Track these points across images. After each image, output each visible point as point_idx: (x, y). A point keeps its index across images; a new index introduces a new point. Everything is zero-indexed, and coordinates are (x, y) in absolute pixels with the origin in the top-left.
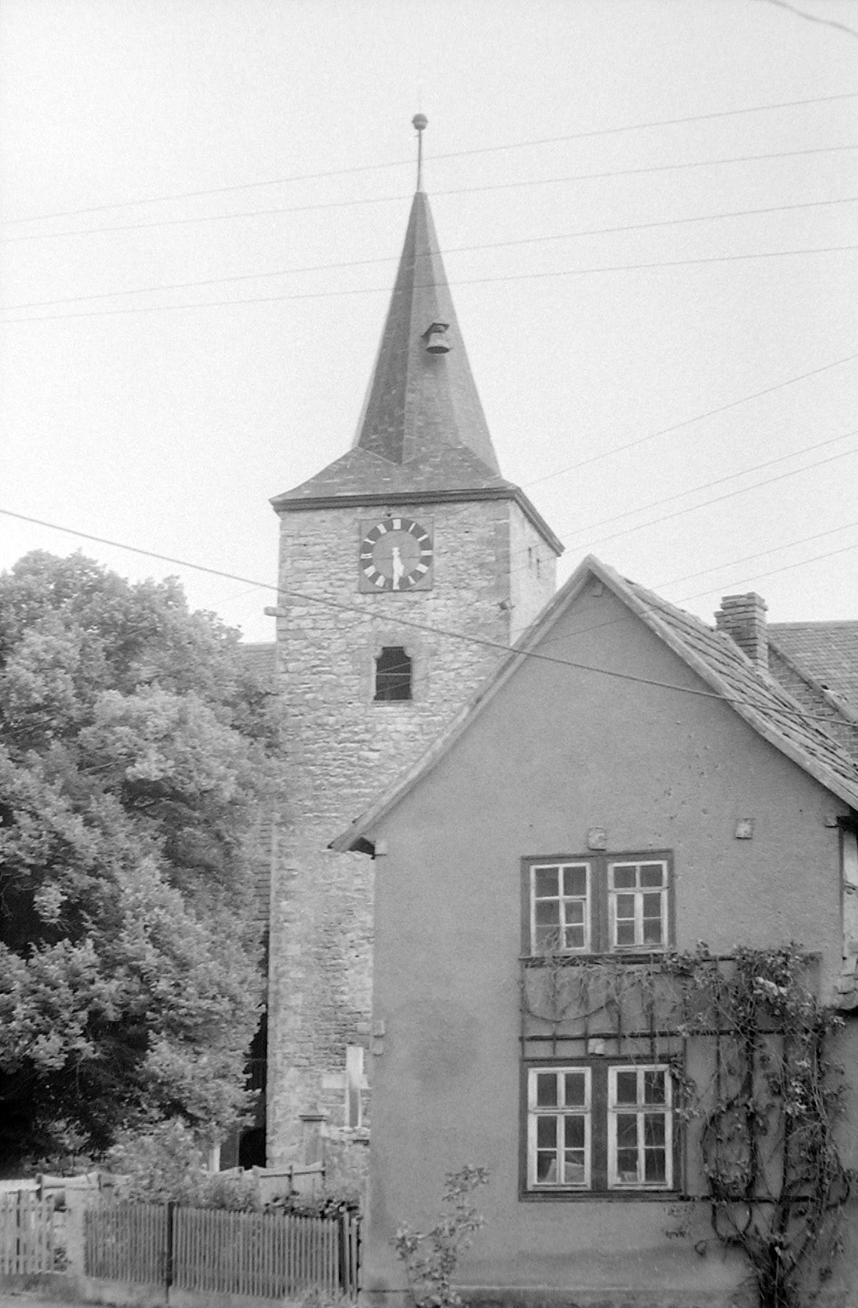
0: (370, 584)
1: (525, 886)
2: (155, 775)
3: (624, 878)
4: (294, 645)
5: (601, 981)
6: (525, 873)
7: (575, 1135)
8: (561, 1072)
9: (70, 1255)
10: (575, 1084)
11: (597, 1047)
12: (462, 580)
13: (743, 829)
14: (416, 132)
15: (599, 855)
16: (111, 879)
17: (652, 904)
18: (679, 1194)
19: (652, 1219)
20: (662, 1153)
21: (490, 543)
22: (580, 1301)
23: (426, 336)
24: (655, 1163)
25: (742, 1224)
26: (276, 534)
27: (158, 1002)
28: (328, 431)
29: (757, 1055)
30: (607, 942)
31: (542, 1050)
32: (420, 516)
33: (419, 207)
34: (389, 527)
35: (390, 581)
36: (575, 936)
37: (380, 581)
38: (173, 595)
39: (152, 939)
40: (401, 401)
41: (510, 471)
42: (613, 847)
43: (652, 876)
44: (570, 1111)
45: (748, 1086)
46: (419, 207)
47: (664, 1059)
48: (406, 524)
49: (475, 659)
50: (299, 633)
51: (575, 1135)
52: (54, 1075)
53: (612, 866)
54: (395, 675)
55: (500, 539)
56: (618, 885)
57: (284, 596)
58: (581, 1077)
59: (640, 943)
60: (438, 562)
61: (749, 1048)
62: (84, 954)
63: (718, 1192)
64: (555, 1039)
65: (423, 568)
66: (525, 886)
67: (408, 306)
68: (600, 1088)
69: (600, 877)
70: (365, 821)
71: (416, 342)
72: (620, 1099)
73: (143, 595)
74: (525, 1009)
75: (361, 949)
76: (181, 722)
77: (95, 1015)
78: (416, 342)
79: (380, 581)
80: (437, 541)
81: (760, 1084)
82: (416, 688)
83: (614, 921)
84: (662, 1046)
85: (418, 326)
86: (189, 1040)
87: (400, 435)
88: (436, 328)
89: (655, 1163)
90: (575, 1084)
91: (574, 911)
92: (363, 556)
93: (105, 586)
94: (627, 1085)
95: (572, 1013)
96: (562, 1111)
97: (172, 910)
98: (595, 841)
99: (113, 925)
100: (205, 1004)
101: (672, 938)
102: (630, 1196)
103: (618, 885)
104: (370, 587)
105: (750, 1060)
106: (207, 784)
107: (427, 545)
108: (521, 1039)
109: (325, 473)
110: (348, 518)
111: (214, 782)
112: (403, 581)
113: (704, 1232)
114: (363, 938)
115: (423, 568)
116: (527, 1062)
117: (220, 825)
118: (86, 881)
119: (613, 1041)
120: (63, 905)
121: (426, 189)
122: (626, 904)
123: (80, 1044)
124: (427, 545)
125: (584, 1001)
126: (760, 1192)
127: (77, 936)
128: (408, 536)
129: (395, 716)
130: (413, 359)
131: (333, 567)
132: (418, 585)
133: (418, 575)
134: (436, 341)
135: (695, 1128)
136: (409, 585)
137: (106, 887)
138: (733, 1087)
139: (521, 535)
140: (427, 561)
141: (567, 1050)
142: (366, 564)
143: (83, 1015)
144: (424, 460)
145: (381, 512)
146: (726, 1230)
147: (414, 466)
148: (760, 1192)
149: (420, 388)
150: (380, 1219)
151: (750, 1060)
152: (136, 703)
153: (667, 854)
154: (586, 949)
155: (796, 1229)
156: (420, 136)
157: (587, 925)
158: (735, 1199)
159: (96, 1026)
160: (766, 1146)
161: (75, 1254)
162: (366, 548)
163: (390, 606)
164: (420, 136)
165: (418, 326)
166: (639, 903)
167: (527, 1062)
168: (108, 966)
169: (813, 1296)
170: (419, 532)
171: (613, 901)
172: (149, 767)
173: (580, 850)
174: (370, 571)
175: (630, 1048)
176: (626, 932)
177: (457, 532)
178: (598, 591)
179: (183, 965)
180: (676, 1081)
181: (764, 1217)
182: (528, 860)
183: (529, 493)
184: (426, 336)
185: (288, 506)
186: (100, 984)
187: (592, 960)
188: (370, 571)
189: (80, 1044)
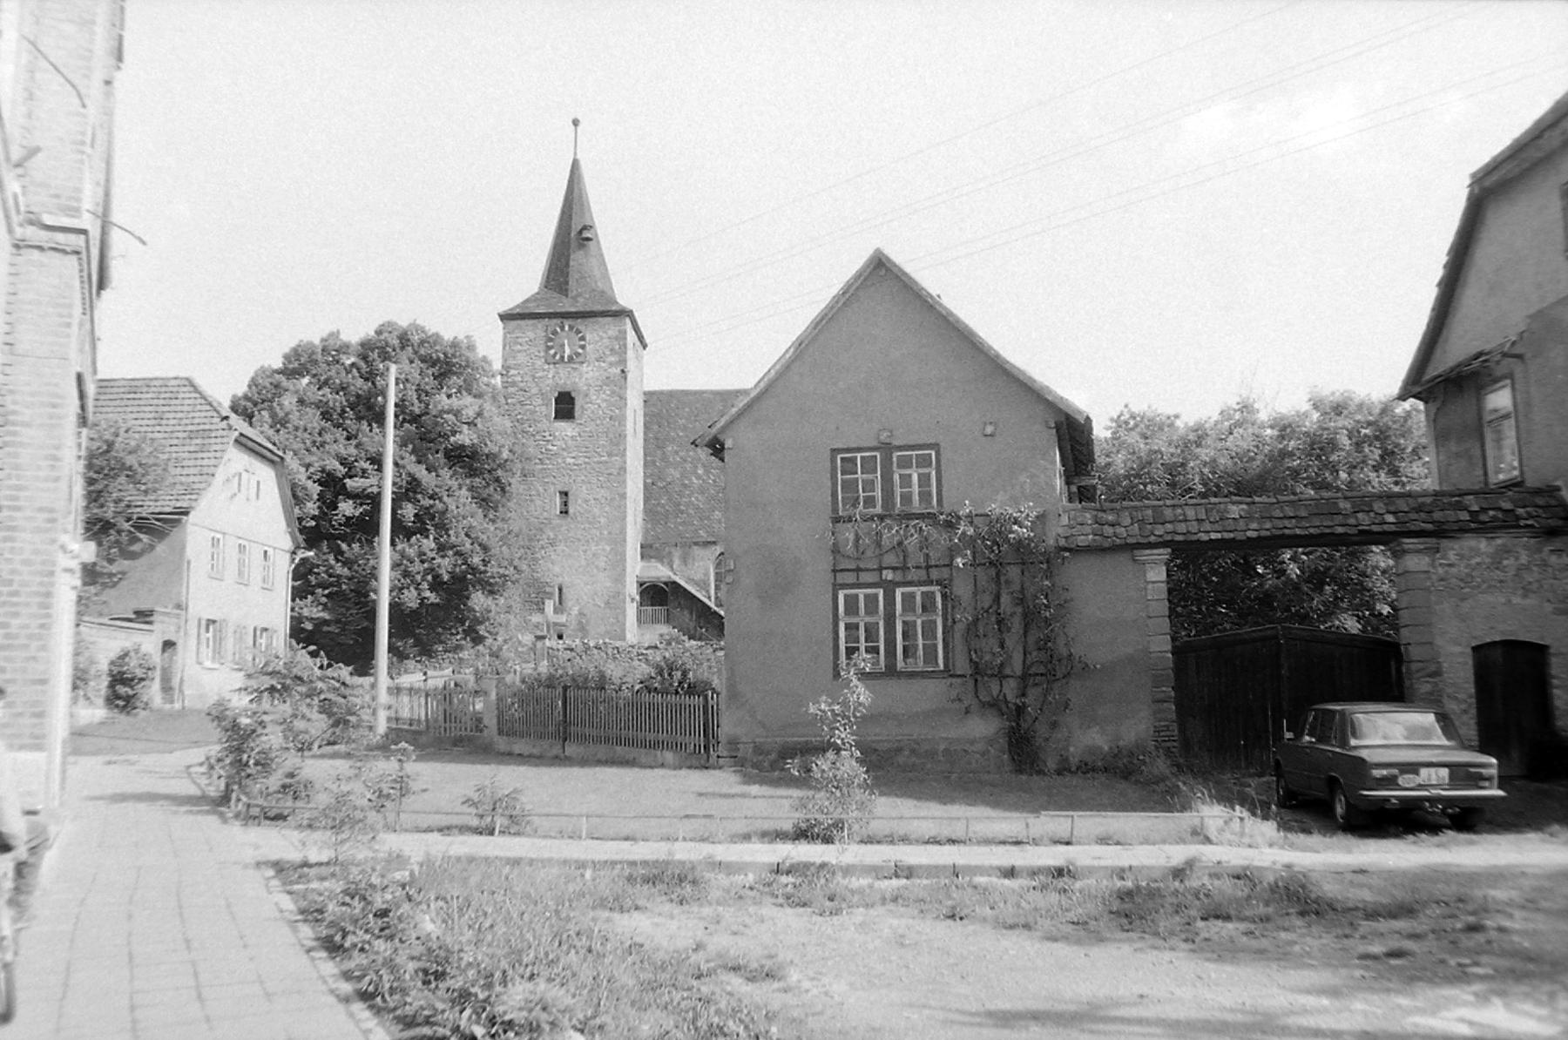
1: (834, 469)
2: (467, 442)
3: (905, 463)
4: (511, 390)
5: (891, 534)
6: (833, 461)
7: (871, 634)
8: (861, 593)
9: (486, 721)
10: (871, 601)
11: (888, 575)
13: (989, 430)
15: (887, 448)
16: (440, 499)
17: (925, 480)
18: (948, 672)
19: (931, 693)
20: (935, 646)
21: (616, 338)
23: (580, 232)
24: (930, 652)
25: (995, 693)
26: (501, 332)
27: (474, 570)
28: (524, 278)
29: (1003, 579)
30: (894, 505)
31: (850, 578)
32: (580, 324)
33: (575, 165)
34: (562, 328)
35: (562, 357)
36: (870, 502)
38: (471, 347)
39: (467, 535)
40: (567, 265)
41: (624, 299)
42: (896, 443)
43: (924, 462)
44: (868, 619)
45: (997, 598)
46: (575, 165)
47: (939, 583)
48: (571, 328)
50: (514, 384)
51: (871, 634)
52: (413, 612)
53: (896, 454)
54: (565, 406)
55: (622, 336)
56: (899, 467)
58: (876, 596)
59: (916, 505)
60: (588, 348)
61: (998, 575)
62: (429, 544)
63: (978, 671)
64: (858, 570)
66: (834, 469)
67: (570, 217)
68: (889, 601)
69: (887, 462)
70: (719, 425)
71: (573, 237)
72: (904, 609)
73: (455, 344)
74: (836, 550)
76: (479, 414)
77: (437, 577)
78: (573, 237)
81: (1005, 599)
82: (577, 413)
83: (898, 491)
84: (935, 574)
85: (576, 227)
86: (492, 592)
87: (567, 283)
88: (585, 228)
89: (930, 652)
90: (871, 601)
91: (868, 486)
93: (432, 340)
94: (908, 599)
95: (869, 553)
96: (862, 620)
97: (477, 520)
98: (884, 436)
99: (442, 527)
100: (502, 571)
101: (940, 501)
102: (912, 675)
103: (899, 467)
105: (998, 582)
106: (495, 450)
107: (583, 339)
108: (834, 571)
109: (527, 301)
110: (541, 324)
112: (571, 358)
113: (969, 700)
116: (837, 587)
117: (500, 472)
118: (427, 502)
119: (899, 572)
120: (416, 515)
121: (579, 157)
122: (906, 480)
123: (428, 594)
124: (583, 339)
125: (879, 545)
126: (1008, 671)
127: (424, 532)
128: (573, 334)
129: (565, 428)
130: (574, 244)
131: (533, 350)
133: (578, 355)
134: (586, 234)
135: (960, 627)
137: (439, 506)
138: (986, 600)
139: (631, 336)
140: (583, 347)
141: (866, 577)
142: (550, 348)
143: (429, 577)
144: (579, 295)
145: (558, 321)
146: (984, 697)
147: (574, 298)
148: (1008, 671)
149: (577, 258)
150: (734, 695)
151: (998, 582)
152: (455, 402)
153: (935, 446)
154: (878, 510)
155: (1033, 695)
157: (878, 493)
158: (993, 675)
159: (437, 584)
160: (1012, 640)
161: (490, 721)
163: (563, 371)
165: (576, 227)
166: (915, 477)
167: (837, 587)
168: (442, 548)
169: (1047, 739)
171: (896, 477)
172: (465, 437)
173: (874, 443)
175: (913, 575)
176: (907, 498)
177: (597, 335)
178: (883, 272)
179: (485, 548)
180: (944, 596)
181: (1010, 689)
182: (835, 451)
183: (636, 314)
184: (580, 232)
185: (506, 317)
186: (439, 560)
187: (882, 518)
189: (428, 594)
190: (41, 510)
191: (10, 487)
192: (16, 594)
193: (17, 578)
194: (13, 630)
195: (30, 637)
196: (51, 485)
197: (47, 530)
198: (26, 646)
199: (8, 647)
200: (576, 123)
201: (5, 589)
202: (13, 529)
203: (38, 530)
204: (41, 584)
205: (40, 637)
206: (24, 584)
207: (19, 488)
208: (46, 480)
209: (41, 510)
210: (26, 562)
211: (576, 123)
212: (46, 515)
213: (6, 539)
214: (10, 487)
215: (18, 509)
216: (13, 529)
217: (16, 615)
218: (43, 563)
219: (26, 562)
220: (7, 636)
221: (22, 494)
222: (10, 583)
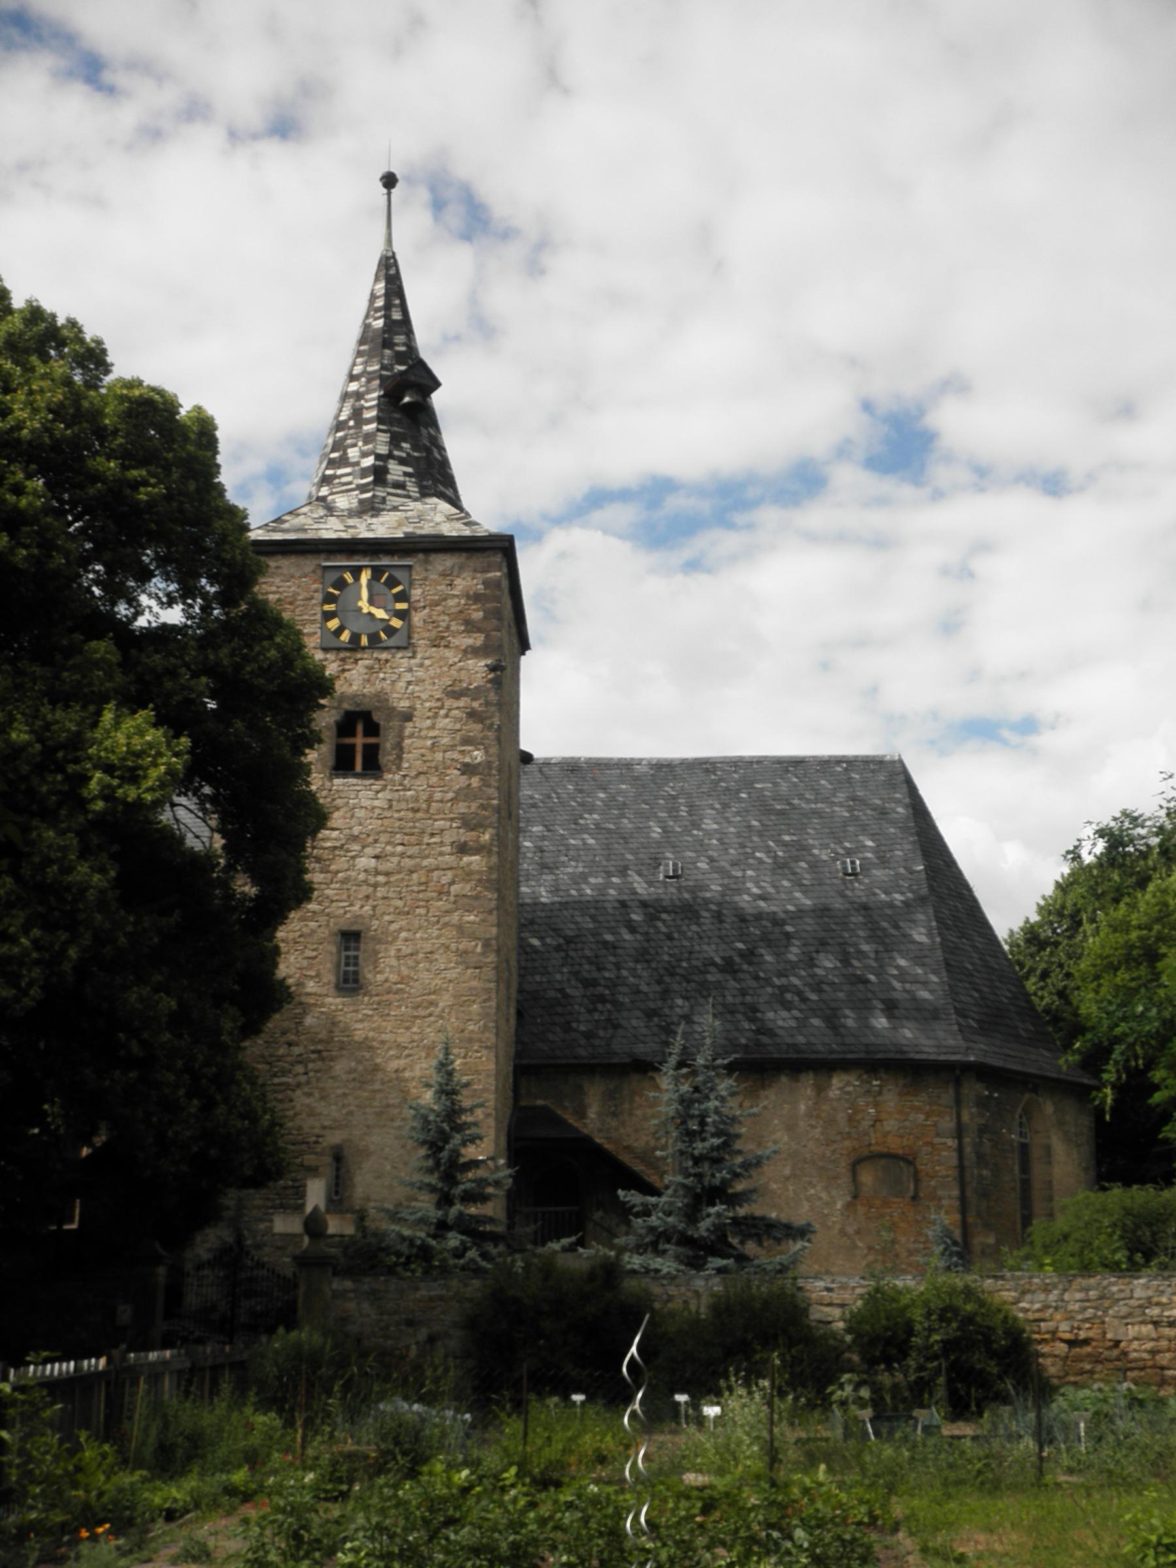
0: (333, 637)
12: (443, 638)
14: (385, 191)
22: (182, 839)
37: (345, 636)
49: (458, 726)
57: (984, 1239)
60: (417, 618)
65: (396, 623)
75: (311, 1066)
79: (345, 636)
80: (416, 593)
92: (327, 607)
104: (333, 643)
111: (366, 1287)
114: (313, 1052)
115: (396, 623)
132: (393, 642)
136: (379, 640)
142: (328, 616)
156: (389, 194)
162: (329, 599)
164: (389, 194)
170: (392, 582)
174: (333, 624)
188: (333, 624)
211: (389, 181)
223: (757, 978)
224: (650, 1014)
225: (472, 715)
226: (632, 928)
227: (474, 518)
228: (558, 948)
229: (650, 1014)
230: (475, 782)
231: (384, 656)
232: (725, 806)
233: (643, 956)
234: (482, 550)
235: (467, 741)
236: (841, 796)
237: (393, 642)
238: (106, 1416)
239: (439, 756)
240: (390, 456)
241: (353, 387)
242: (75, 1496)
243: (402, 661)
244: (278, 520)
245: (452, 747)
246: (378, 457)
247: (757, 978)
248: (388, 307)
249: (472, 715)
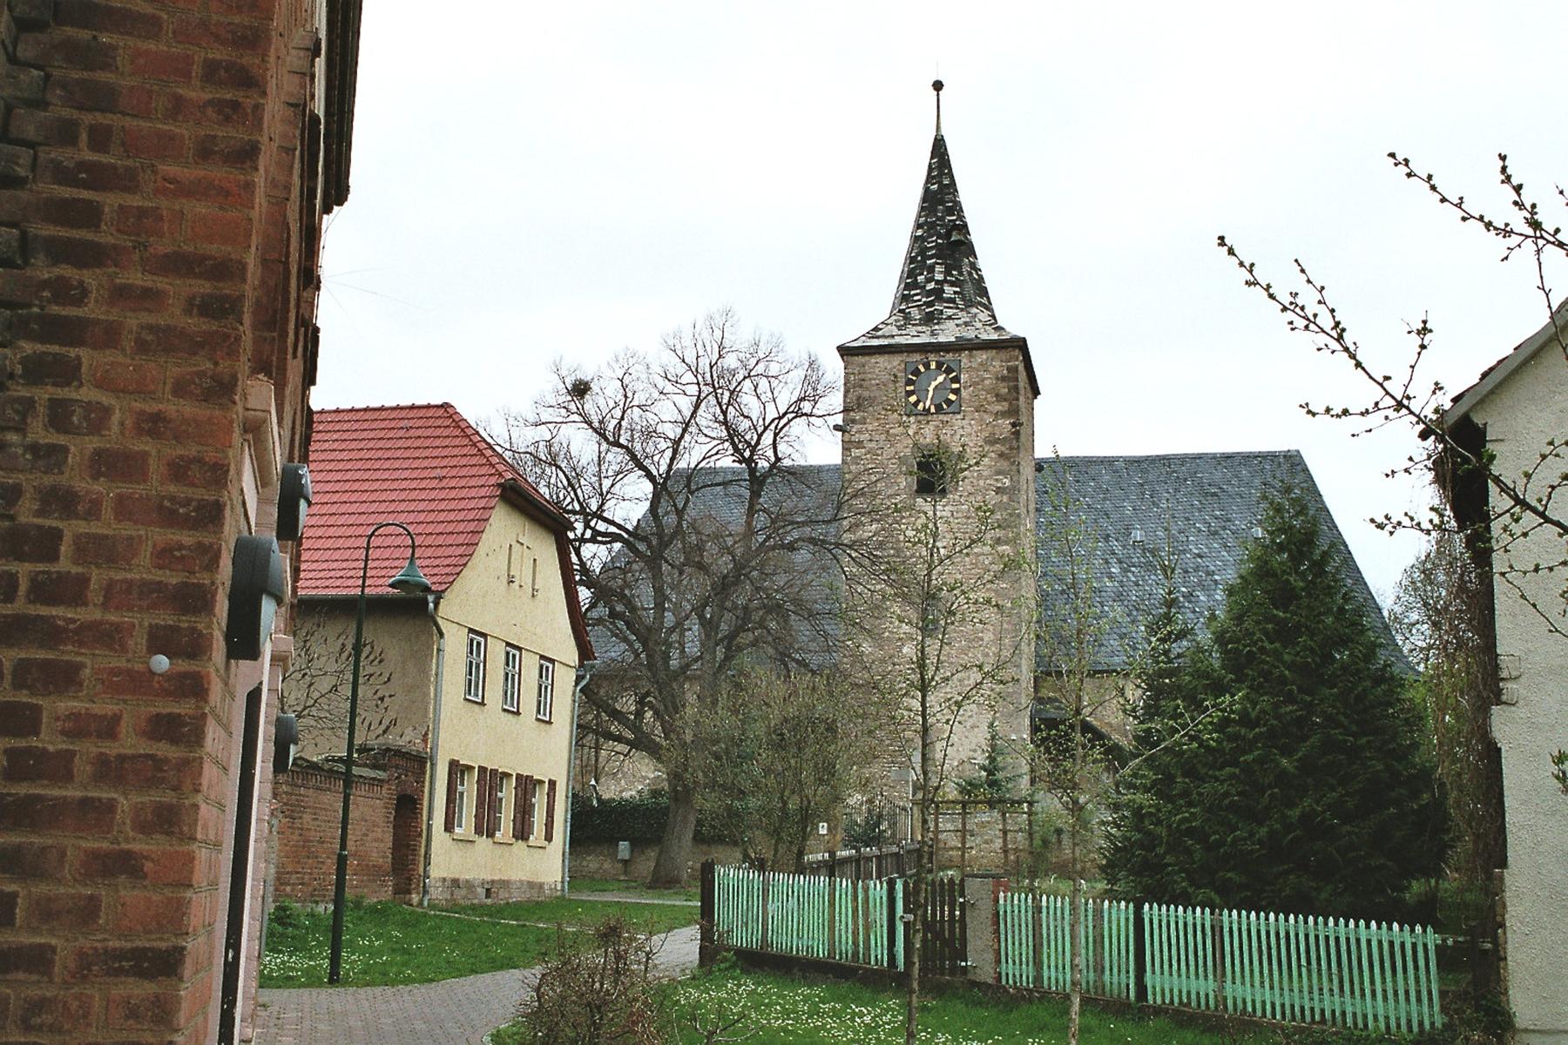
4: (855, 452)
28: (868, 297)
33: (939, 148)
34: (927, 366)
46: (939, 148)
50: (860, 444)
60: (964, 393)
71: (942, 242)
78: (942, 242)
107: (956, 380)
115: (952, 397)
140: (956, 392)
145: (917, 357)
162: (909, 382)
174: (913, 399)
182: (550, 722)
188: (913, 399)
190: (180, 264)
191: (63, 175)
192: (70, 591)
193: (71, 529)
194: (48, 740)
195: (111, 771)
196: (217, 173)
197: (195, 345)
198: (95, 813)
199: (24, 814)
200: (938, 86)
201: (24, 570)
202: (72, 332)
203: (163, 341)
204: (165, 556)
205: (151, 772)
206: (96, 550)
207: (100, 178)
208: (205, 152)
209: (180, 264)
210: (108, 464)
211: (938, 86)
212: (203, 287)
213: (37, 371)
214: (63, 175)
215: (92, 256)
216: (72, 332)
217: (64, 678)
218: (178, 471)
219: (108, 464)
220: (23, 766)
221: (110, 201)
222: (47, 545)
223: (1194, 612)
224: (1122, 636)
225: (1001, 455)
226: (1111, 577)
227: (1000, 323)
228: (1063, 592)
229: (1122, 636)
230: (1005, 499)
231: (945, 418)
232: (1176, 490)
233: (1119, 597)
234: (1006, 348)
235: (998, 473)
236: (1257, 482)
237: (951, 409)
238: (288, 311)
239: (981, 483)
240: (945, 281)
241: (919, 233)
242: (685, 820)
243: (957, 420)
244: (876, 329)
245: (990, 477)
246: (937, 282)
247: (1194, 612)
248: (941, 174)
249: (1001, 455)
